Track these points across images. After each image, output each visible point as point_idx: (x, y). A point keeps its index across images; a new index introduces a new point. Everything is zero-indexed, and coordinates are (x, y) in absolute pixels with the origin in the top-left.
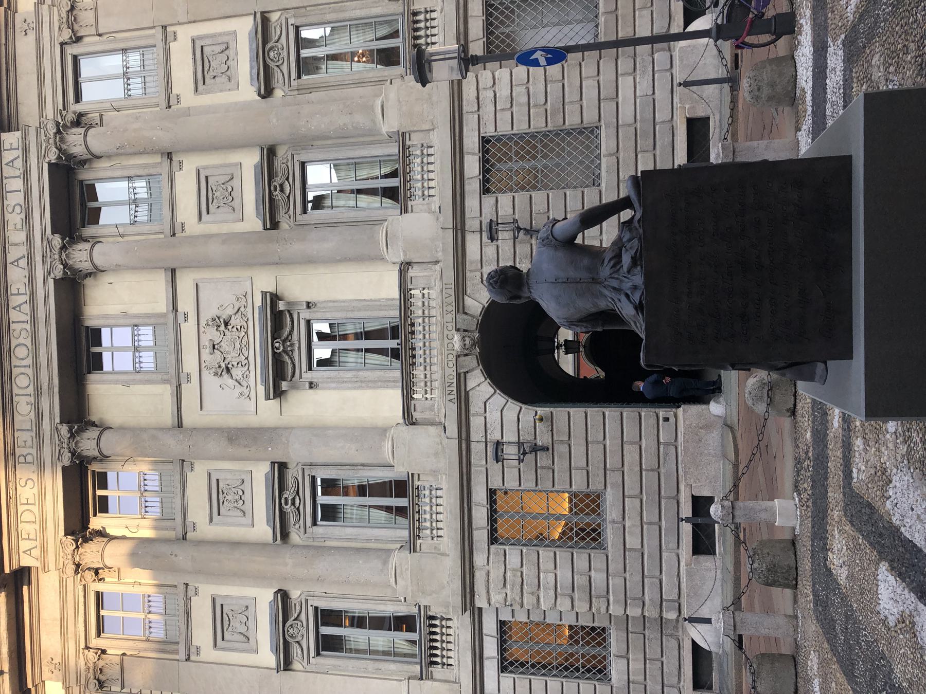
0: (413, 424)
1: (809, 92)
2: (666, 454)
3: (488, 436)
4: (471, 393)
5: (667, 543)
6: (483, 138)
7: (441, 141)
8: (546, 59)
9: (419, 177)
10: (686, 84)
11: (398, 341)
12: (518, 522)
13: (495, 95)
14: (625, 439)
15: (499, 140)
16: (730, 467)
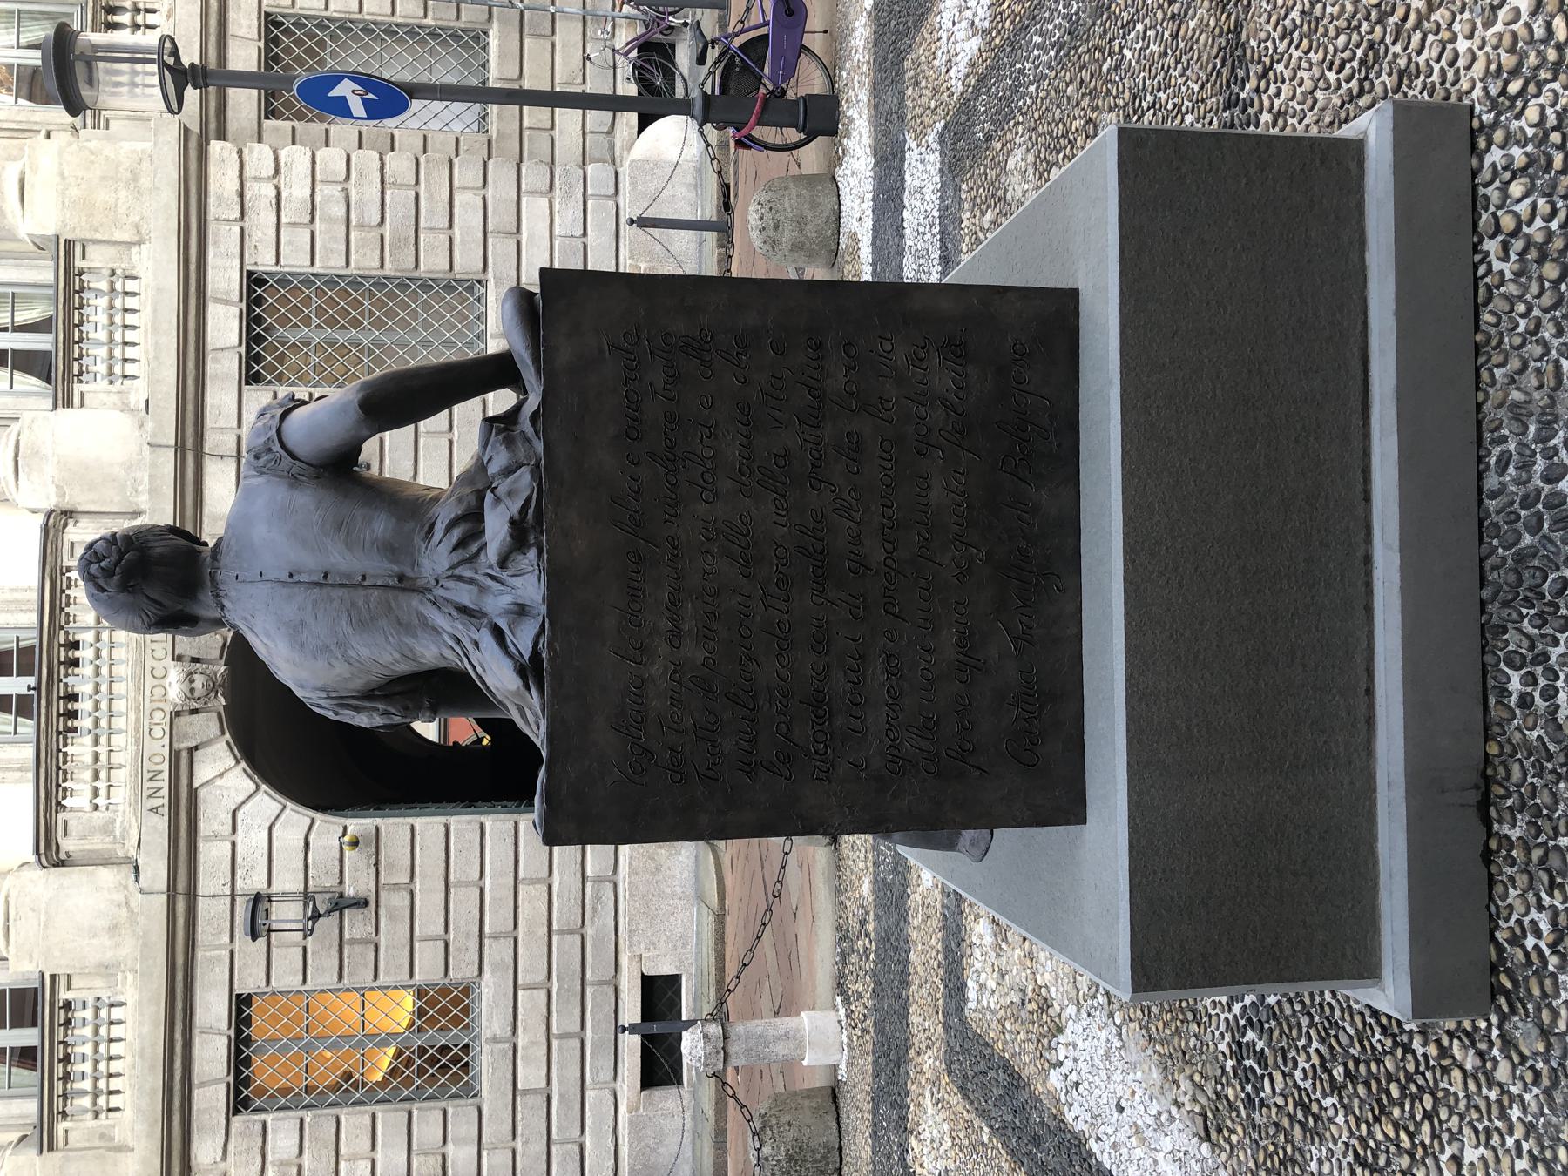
0: (61, 864)
1: (866, 237)
2: (597, 899)
3: (239, 881)
4: (202, 793)
5: (596, 1072)
6: (250, 273)
7: (156, 270)
8: (365, 102)
9: (102, 335)
10: (643, 223)
11: (32, 680)
12: (297, 1059)
13: (278, 195)
14: (521, 875)
15: (283, 281)
16: (709, 922)
